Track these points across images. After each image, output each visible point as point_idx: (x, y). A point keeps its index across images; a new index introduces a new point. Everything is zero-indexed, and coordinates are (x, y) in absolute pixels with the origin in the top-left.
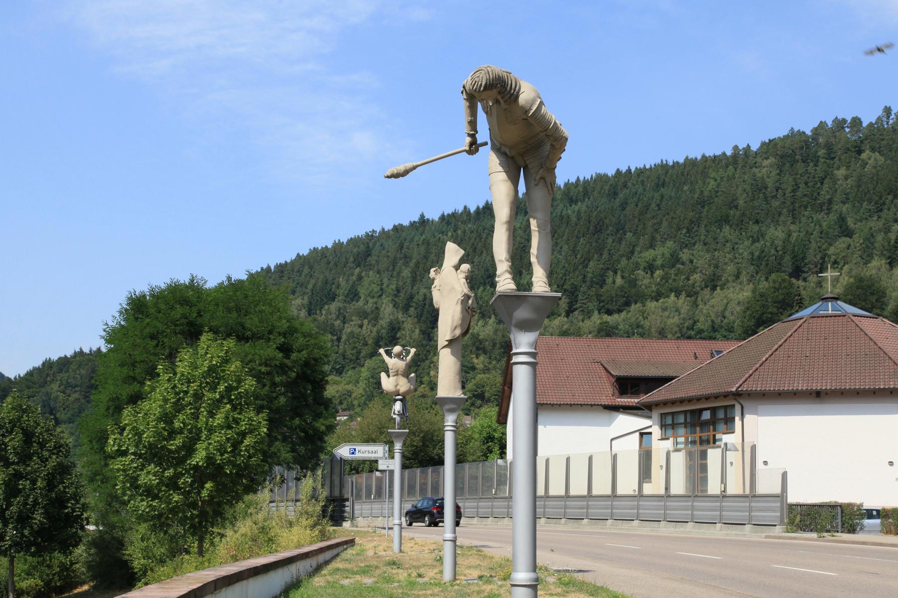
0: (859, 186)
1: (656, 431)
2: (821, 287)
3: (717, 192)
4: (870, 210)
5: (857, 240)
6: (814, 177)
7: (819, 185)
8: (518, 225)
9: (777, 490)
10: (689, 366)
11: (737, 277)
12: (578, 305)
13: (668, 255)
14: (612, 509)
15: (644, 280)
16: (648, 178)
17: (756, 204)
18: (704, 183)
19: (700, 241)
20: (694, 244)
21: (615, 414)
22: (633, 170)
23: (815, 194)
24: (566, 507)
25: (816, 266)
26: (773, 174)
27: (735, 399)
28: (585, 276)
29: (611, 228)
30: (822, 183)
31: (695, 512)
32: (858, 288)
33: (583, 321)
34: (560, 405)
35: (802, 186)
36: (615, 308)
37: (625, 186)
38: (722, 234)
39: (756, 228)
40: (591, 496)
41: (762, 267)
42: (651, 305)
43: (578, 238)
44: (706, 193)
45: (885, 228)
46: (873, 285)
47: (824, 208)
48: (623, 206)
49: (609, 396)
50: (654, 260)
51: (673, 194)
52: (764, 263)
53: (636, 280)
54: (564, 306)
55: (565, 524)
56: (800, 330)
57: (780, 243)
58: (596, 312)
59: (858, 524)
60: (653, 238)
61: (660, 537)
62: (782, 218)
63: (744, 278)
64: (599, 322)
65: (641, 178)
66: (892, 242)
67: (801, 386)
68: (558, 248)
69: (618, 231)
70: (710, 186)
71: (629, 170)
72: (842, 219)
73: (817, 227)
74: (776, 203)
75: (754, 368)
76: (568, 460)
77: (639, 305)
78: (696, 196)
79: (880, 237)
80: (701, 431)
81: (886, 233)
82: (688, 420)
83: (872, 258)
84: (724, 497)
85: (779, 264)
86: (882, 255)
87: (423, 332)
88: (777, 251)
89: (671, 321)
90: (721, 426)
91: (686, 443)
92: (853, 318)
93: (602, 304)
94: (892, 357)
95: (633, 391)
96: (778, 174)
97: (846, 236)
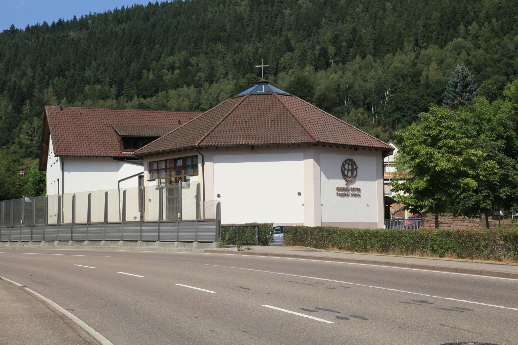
0: (298, 21)
1: (146, 175)
2: (277, 83)
3: (213, 20)
4: (304, 36)
5: (297, 53)
6: (271, 14)
7: (274, 19)
8: (82, 36)
9: (214, 217)
10: (170, 127)
11: (226, 75)
12: (124, 92)
13: (182, 60)
14: (44, 234)
15: (168, 77)
16: (169, 9)
17: (237, 29)
18: (205, 14)
19: (203, 51)
20: (199, 53)
21: (121, 163)
22: (159, 4)
23: (272, 24)
24: (72, 232)
25: (273, 70)
26: (247, 10)
27: (198, 151)
28: (128, 73)
29: (145, 41)
30: (276, 18)
31: (161, 234)
32: (297, 83)
33: (127, 102)
34: (80, 157)
35: (264, 19)
36: (149, 94)
37: (154, 13)
38: (216, 48)
39: (237, 44)
40: (91, 224)
41: (241, 69)
42: (172, 92)
43: (124, 47)
44: (206, 21)
45: (313, 47)
46: (306, 82)
47: (278, 33)
48: (153, 27)
49: (116, 150)
50: (174, 63)
51: (185, 21)
52: (242, 67)
53: (162, 76)
54: (114, 92)
55: (72, 245)
56: (243, 103)
57: (251, 55)
58: (136, 97)
59: (269, 238)
60: (173, 49)
61: (137, 254)
62: (253, 39)
63: (230, 76)
64: (137, 103)
65: (165, 9)
66: (317, 56)
67: (242, 142)
68: (110, 53)
69: (150, 43)
70: (209, 16)
71: (157, 3)
72: (288, 41)
73: (274, 45)
74: (249, 29)
75: (211, 130)
76: (90, 196)
77: (163, 92)
78: (200, 23)
79: (309, 53)
80: (177, 174)
81: (313, 50)
82: (168, 167)
83: (306, 65)
84: (180, 222)
85: (251, 68)
86: (311, 63)
87: (14, 108)
88: (250, 60)
89: (184, 103)
90: (190, 171)
91: (166, 182)
92: (277, 96)
93: (140, 92)
94: (300, 122)
95: (132, 147)
96: (250, 11)
97: (290, 51)
